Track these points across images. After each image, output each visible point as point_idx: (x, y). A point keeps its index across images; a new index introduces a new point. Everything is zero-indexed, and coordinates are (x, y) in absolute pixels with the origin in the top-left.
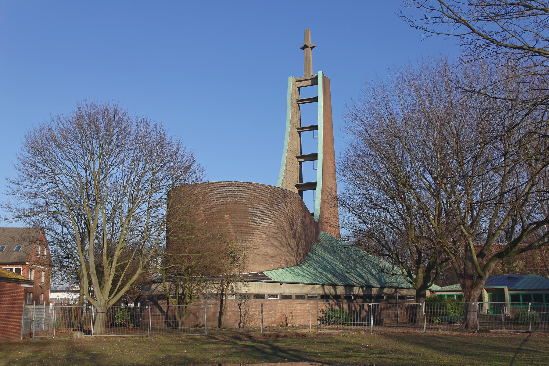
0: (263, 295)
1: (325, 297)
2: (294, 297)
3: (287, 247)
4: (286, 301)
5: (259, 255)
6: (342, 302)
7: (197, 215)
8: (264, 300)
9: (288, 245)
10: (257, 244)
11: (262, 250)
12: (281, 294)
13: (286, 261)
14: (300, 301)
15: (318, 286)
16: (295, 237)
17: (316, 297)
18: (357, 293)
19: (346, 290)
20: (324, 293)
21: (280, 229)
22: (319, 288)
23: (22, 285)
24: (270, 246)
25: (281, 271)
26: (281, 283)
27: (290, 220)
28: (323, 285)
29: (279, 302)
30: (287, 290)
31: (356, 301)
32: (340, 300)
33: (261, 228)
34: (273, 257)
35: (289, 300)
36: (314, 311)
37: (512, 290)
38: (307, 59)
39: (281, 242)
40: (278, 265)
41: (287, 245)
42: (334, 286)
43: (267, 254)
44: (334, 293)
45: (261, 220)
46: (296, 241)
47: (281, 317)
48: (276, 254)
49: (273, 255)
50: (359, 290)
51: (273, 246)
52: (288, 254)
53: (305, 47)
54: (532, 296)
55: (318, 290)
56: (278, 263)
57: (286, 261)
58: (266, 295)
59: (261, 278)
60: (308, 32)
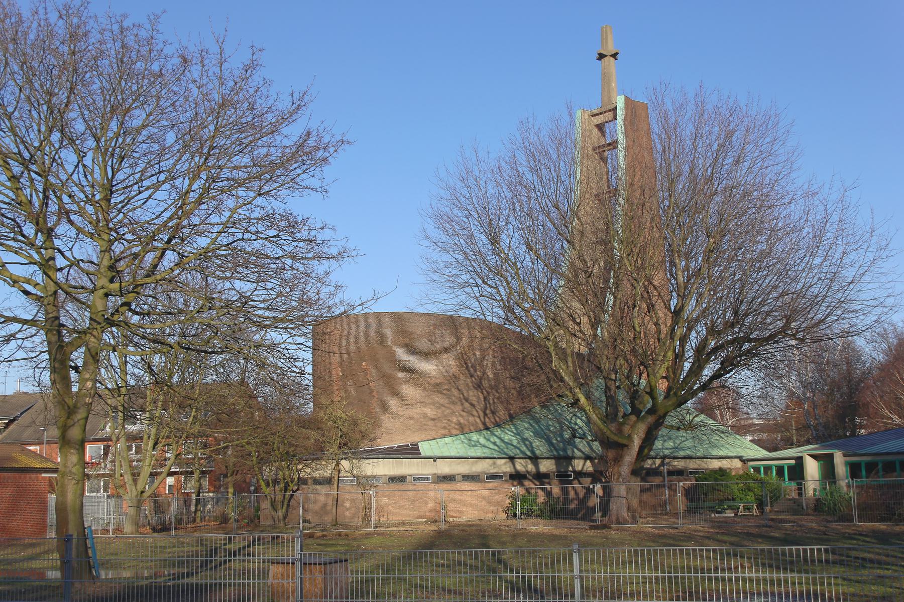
0: (403, 477)
1: (517, 477)
2: (459, 478)
3: (462, 404)
4: (445, 485)
5: (411, 418)
6: (549, 484)
7: (331, 363)
8: (405, 484)
9: (464, 401)
10: (407, 402)
11: (417, 410)
12: (434, 475)
13: (460, 424)
14: (469, 484)
15: (503, 461)
16: (479, 386)
17: (501, 477)
18: (580, 468)
19: (557, 464)
20: (513, 470)
21: (448, 378)
22: (505, 464)
23: (43, 475)
24: (429, 404)
25: (447, 440)
26: (435, 459)
27: (468, 362)
28: (512, 459)
29: (432, 487)
30: (445, 468)
31: (579, 481)
32: (547, 481)
33: (414, 379)
34: (434, 419)
35: (449, 482)
36: (495, 499)
37: (849, 456)
38: (605, 78)
39: (449, 397)
40: (443, 432)
41: (461, 401)
42: (535, 459)
43: (425, 416)
44: (534, 470)
45: (414, 366)
46: (482, 393)
47: (435, 508)
48: (439, 415)
49: (433, 417)
50: (584, 465)
51: (434, 404)
52: (464, 414)
53: (601, 56)
54: (880, 466)
55: (504, 467)
56: (445, 428)
57: (460, 424)
58: (409, 478)
59: (412, 451)
60: (606, 31)
